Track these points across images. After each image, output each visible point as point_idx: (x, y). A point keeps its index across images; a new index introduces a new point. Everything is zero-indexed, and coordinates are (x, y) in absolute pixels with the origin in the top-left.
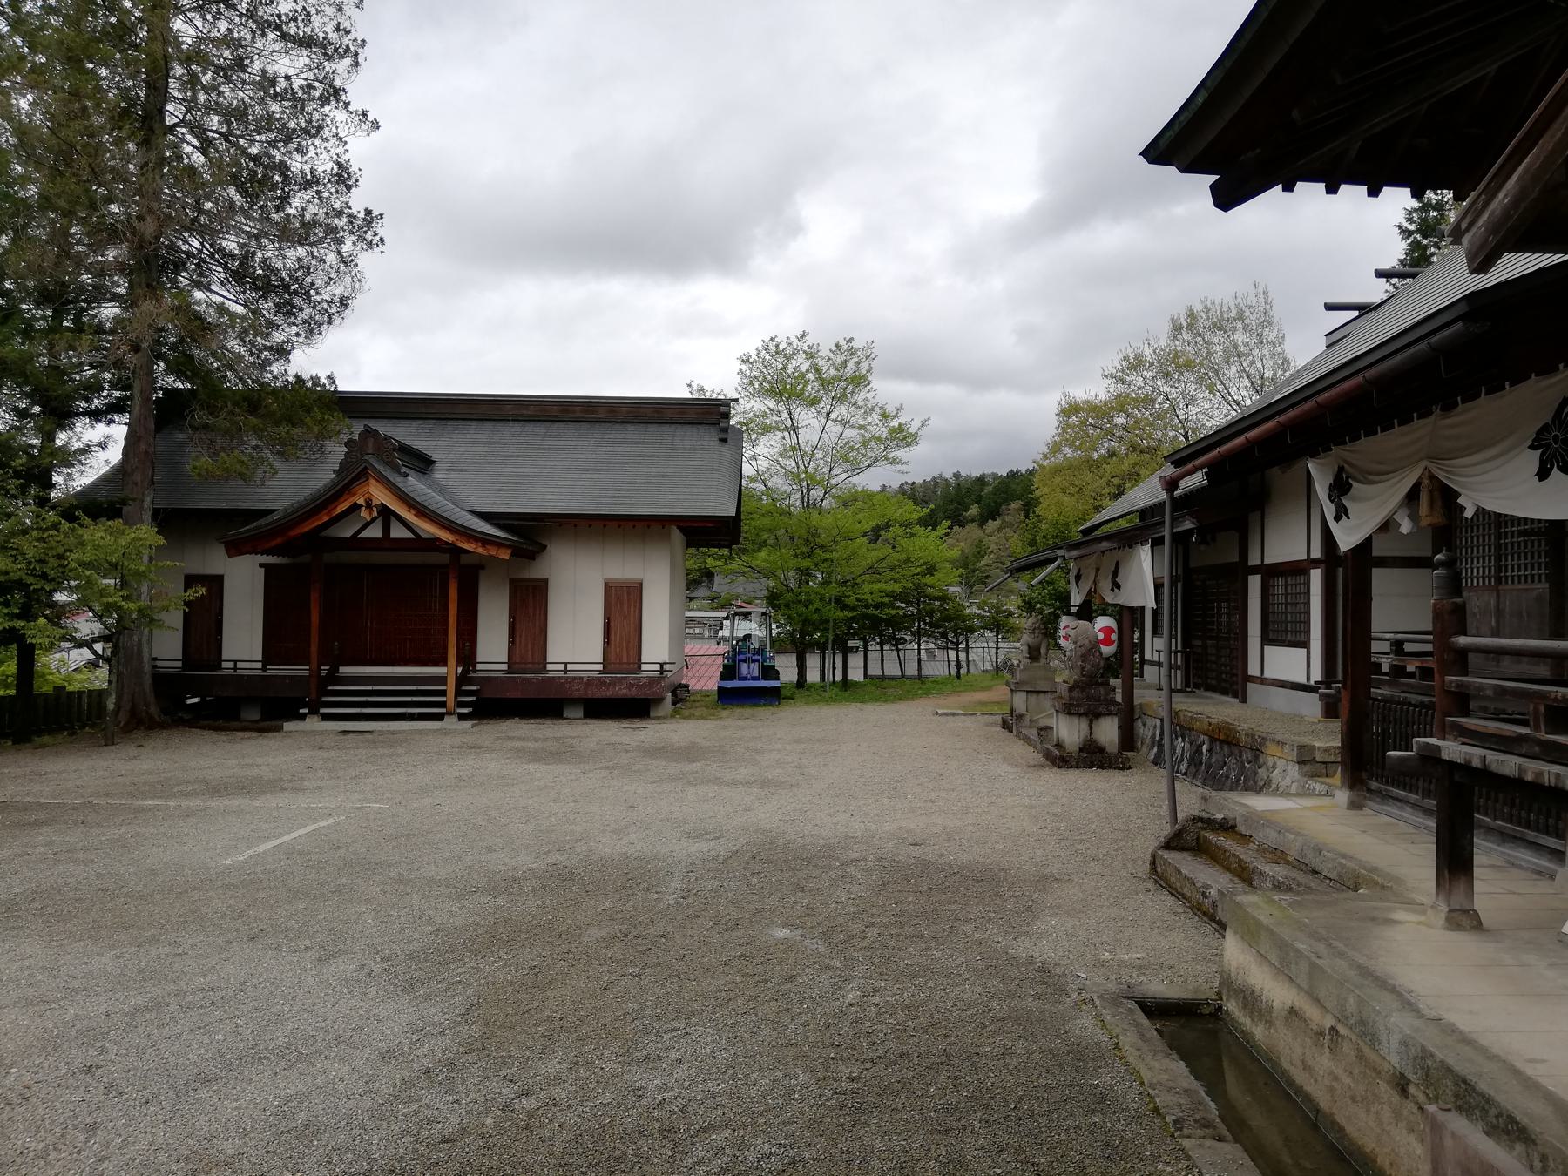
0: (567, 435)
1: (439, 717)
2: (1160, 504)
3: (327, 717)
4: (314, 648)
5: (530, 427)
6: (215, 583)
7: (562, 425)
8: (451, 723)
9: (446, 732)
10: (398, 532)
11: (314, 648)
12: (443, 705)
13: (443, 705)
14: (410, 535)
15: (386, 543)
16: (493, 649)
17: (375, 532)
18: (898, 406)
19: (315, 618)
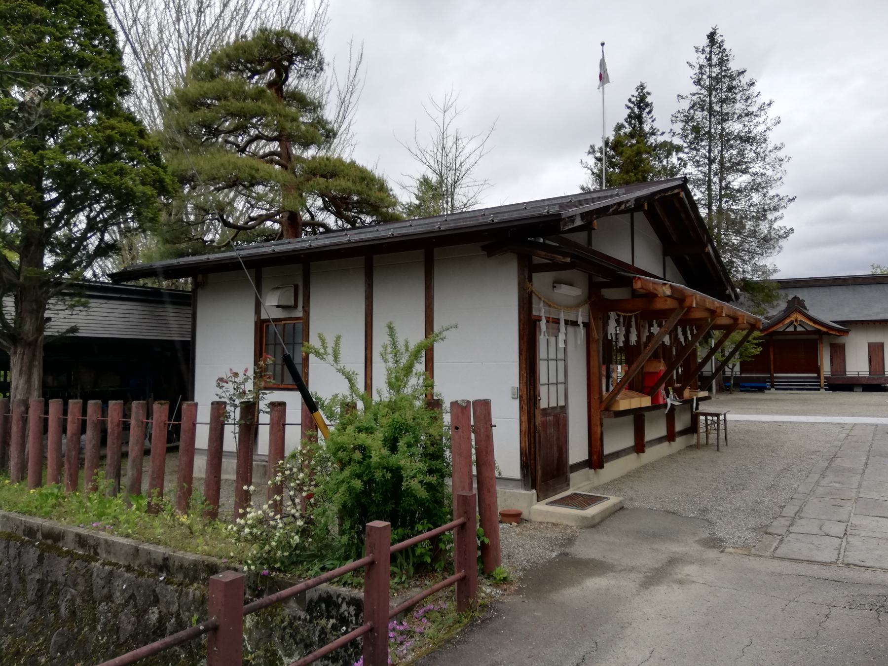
0: (839, 291)
1: (819, 389)
2: (629, 389)
3: (777, 389)
4: (772, 367)
5: (822, 289)
6: (283, 405)
7: (834, 287)
8: (823, 391)
9: (821, 393)
10: (799, 329)
11: (772, 367)
12: (820, 385)
13: (820, 385)
14: (804, 330)
15: (795, 332)
16: (826, 368)
17: (791, 329)
18: (779, 145)
19: (772, 357)
